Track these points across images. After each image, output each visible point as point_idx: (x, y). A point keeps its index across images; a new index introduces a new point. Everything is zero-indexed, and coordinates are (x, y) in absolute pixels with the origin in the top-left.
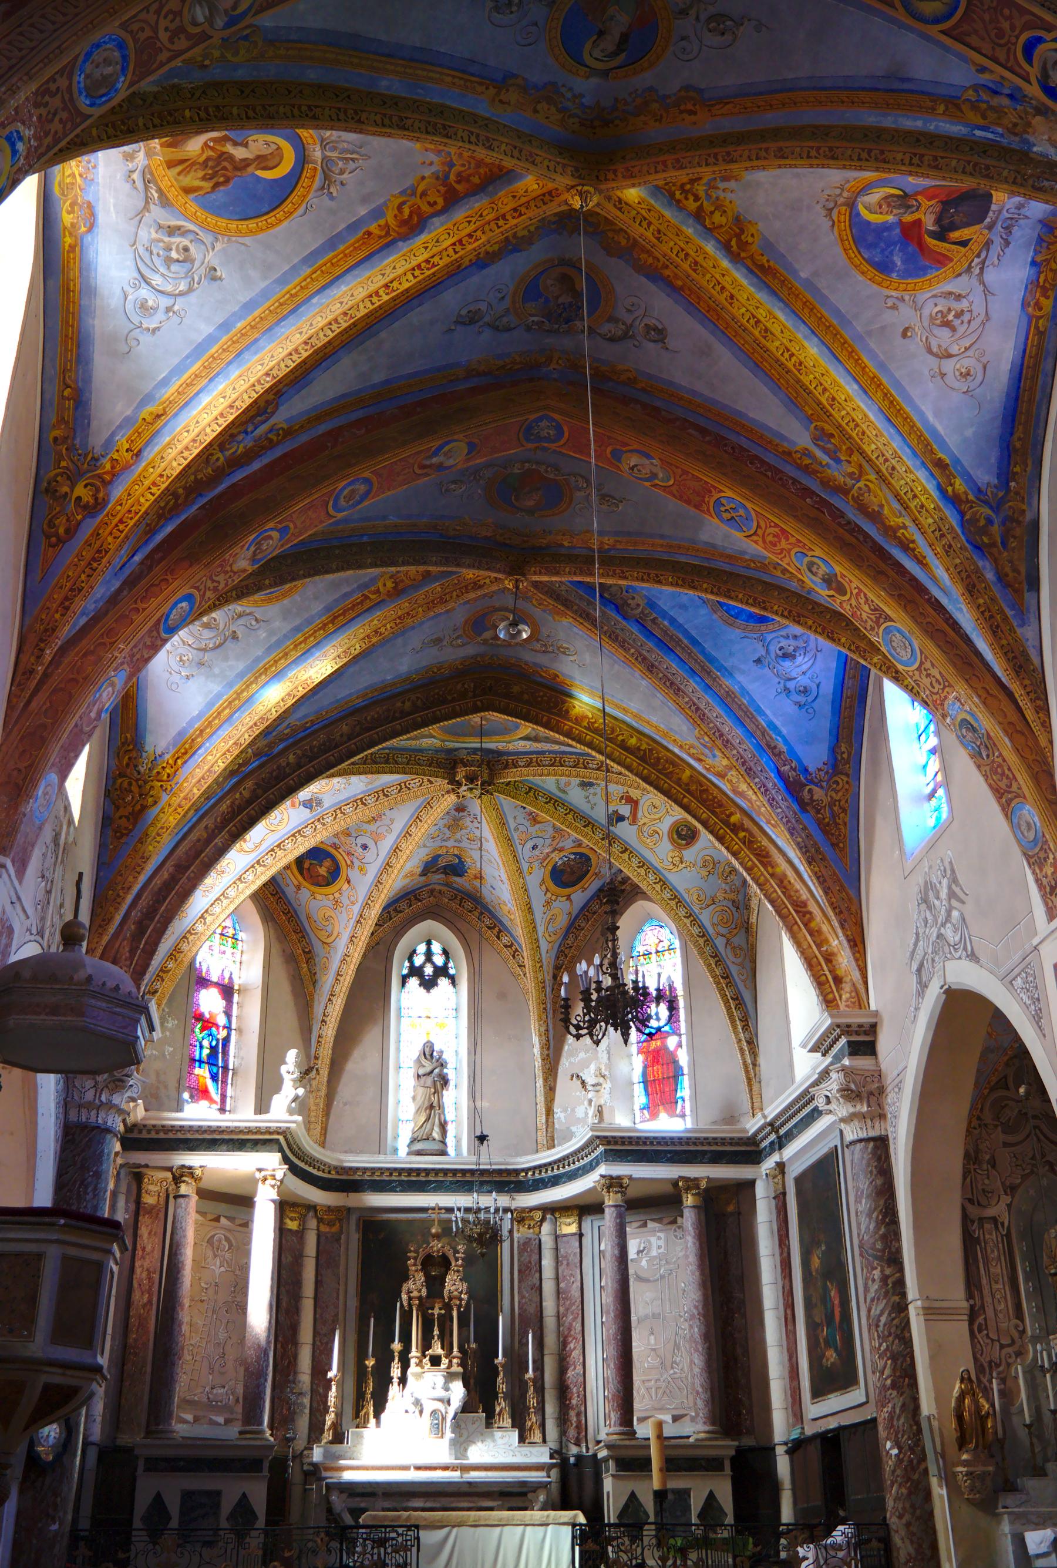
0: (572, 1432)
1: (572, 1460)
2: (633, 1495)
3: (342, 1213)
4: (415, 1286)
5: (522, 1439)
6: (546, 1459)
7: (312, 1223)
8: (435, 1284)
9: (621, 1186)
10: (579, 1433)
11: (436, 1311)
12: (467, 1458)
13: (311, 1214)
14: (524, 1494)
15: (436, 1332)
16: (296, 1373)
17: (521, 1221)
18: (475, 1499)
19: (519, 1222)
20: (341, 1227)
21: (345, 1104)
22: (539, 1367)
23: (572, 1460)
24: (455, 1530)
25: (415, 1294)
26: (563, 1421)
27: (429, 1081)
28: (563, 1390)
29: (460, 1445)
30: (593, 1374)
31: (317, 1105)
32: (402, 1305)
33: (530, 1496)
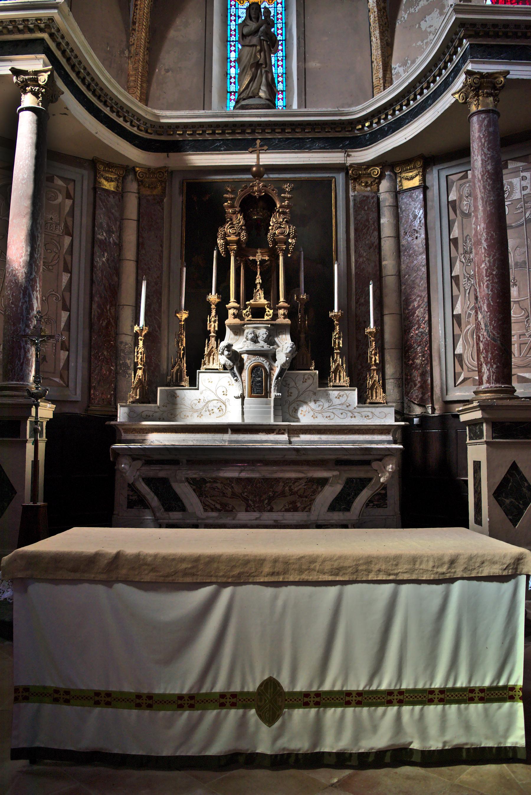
0: (416, 393)
1: (416, 421)
2: (514, 466)
3: (163, 175)
4: (232, 231)
5: (362, 400)
6: (390, 421)
7: (133, 186)
8: (256, 230)
9: (494, 88)
10: (423, 394)
11: (259, 257)
12: (298, 420)
13: (131, 177)
14: (368, 463)
15: (259, 280)
16: (117, 334)
17: (357, 179)
18: (305, 468)
19: (355, 180)
20: (164, 189)
21: (167, 71)
22: (379, 322)
23: (416, 421)
24: (227, 592)
25: (233, 238)
26: (405, 382)
27: (255, 40)
28: (405, 350)
29: (286, 407)
30: (441, 332)
31: (136, 69)
32: (218, 252)
33: (375, 465)
